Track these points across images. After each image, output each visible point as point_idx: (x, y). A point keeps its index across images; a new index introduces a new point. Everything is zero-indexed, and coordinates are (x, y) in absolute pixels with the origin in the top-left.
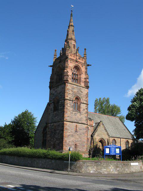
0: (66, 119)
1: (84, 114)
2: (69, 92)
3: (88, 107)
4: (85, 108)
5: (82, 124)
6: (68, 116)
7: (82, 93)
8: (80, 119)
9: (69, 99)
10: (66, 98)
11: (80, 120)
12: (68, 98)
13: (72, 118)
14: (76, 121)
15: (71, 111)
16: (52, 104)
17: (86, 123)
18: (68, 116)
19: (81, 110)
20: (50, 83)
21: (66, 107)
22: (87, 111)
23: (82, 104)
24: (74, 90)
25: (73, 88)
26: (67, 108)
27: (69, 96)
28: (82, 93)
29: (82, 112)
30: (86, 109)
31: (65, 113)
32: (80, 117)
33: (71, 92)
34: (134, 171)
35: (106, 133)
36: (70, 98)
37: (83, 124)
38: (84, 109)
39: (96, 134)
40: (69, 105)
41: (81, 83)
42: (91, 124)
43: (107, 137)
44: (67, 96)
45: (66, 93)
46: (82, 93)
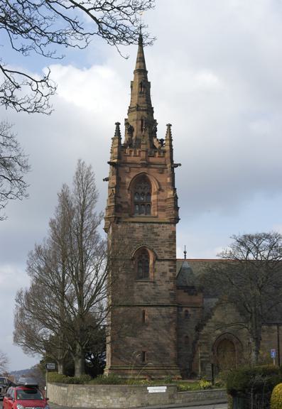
28: (159, 236)
30: (171, 271)
32: (153, 292)
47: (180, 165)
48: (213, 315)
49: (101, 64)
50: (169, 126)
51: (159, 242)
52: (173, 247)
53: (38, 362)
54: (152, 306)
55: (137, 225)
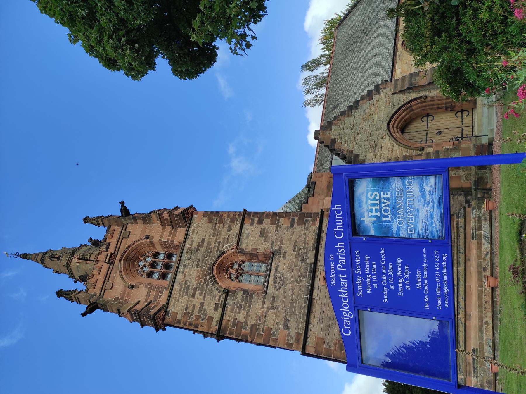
1: (280, 234)
3: (256, 214)
7: (203, 240)
8: (297, 255)
13: (292, 304)
14: (305, 282)
16: (337, 161)
17: (314, 222)
23: (243, 246)
24: (193, 283)
26: (253, 326)
28: (203, 240)
29: (270, 242)
30: (260, 222)
32: (291, 257)
33: (198, 300)
35: (365, 106)
36: (216, 309)
40: (241, 317)
43: (384, 96)
46: (205, 244)
47: (122, 203)
50: (87, 220)
52: (225, 217)
53: (166, 62)
54: (494, 336)
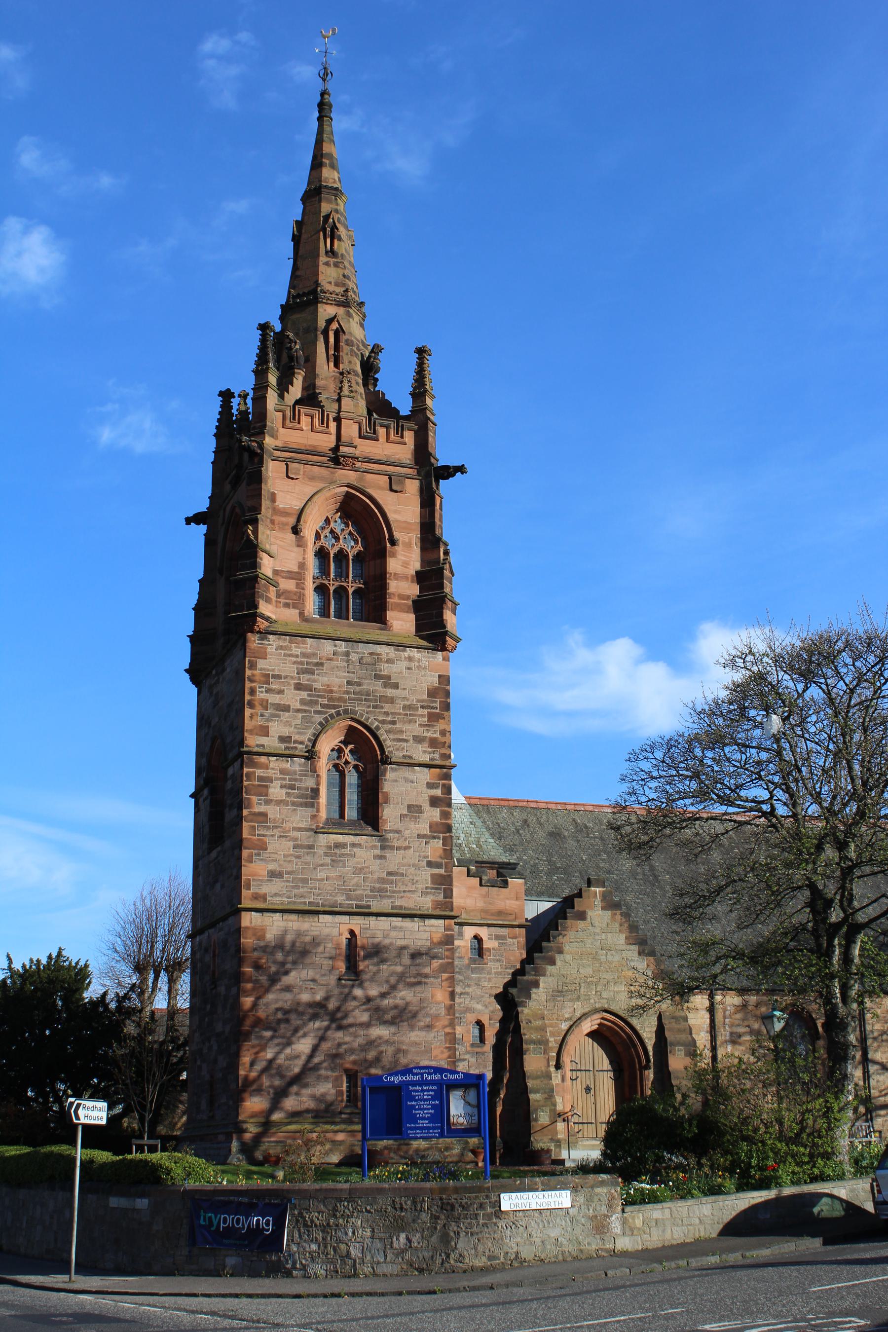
0: (256, 897)
1: (416, 844)
2: (273, 699)
4: (422, 796)
5: (397, 922)
6: (273, 874)
7: (396, 686)
8: (382, 880)
9: (281, 747)
10: (253, 741)
11: (380, 892)
12: (271, 742)
13: (305, 881)
15: (297, 834)
18: (273, 874)
19: (389, 814)
20: (194, 639)
21: (256, 804)
22: (446, 815)
24: (320, 681)
25: (311, 667)
27: (277, 729)
28: (396, 686)
29: (398, 826)
30: (434, 802)
31: (245, 853)
32: (377, 869)
34: (527, 1253)
37: (412, 916)
38: (414, 810)
39: (546, 984)
40: (276, 791)
41: (391, 615)
42: (500, 913)
44: (264, 731)
45: (248, 712)
46: (390, 692)
47: (461, 469)
48: (560, 952)
49: (670, 744)
51: (398, 707)
55: (328, 647)
